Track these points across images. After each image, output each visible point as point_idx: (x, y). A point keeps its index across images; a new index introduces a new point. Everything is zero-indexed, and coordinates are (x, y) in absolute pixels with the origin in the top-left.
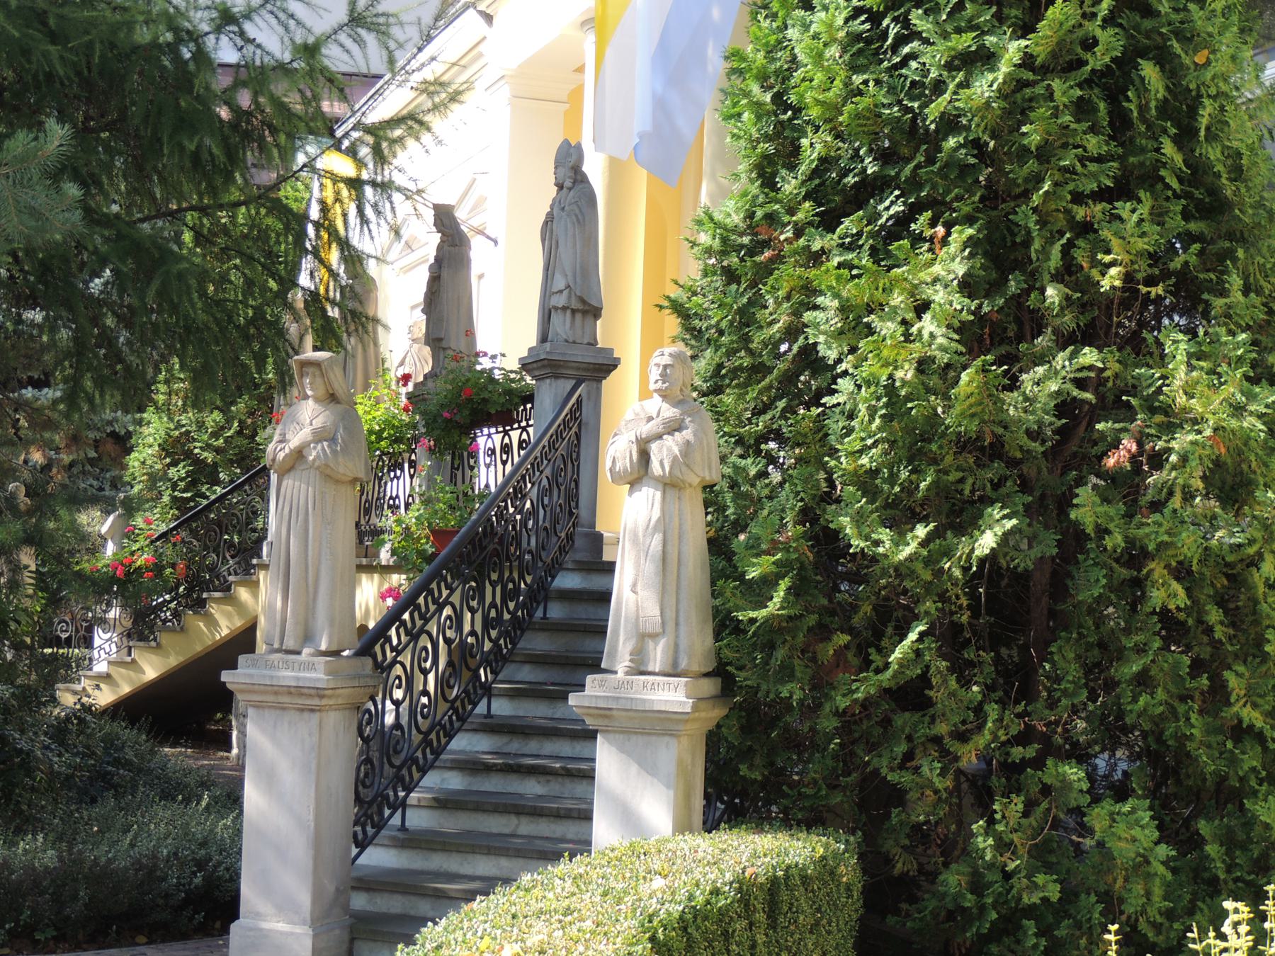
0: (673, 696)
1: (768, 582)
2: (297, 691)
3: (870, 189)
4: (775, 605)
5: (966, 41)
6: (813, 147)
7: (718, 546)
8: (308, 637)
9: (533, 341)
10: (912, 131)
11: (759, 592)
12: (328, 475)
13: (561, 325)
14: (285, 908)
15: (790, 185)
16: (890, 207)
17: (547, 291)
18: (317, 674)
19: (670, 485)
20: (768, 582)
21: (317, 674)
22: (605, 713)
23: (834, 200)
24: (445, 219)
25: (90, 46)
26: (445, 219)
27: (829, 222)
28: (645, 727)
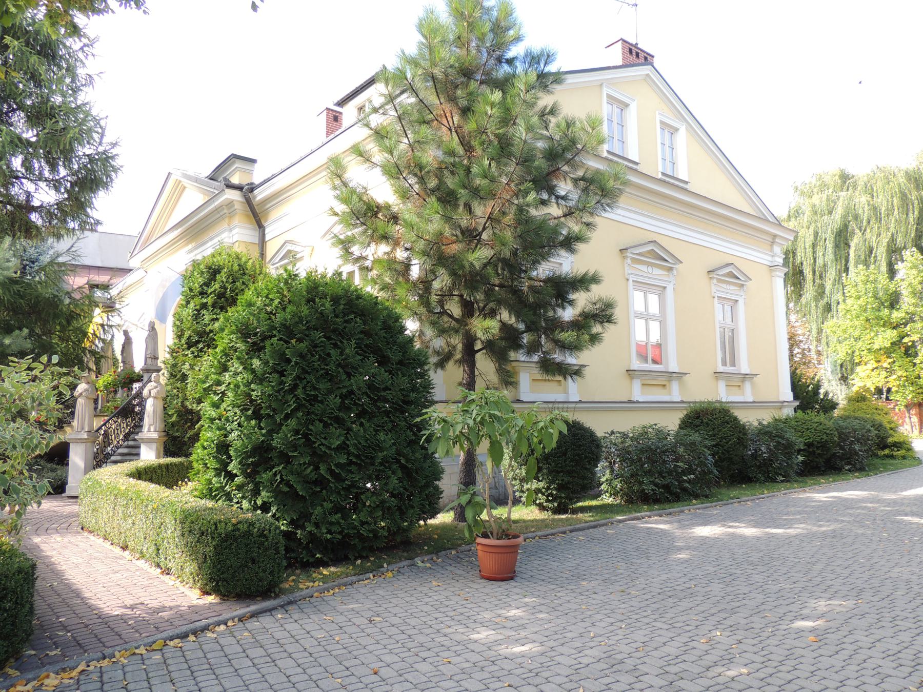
0: (155, 435)
1: (173, 415)
2: (81, 439)
3: (198, 342)
4: (174, 418)
5: (214, 316)
6: (187, 335)
7: (165, 408)
8: (83, 429)
9: (143, 364)
10: (205, 332)
11: (171, 416)
12: (87, 397)
13: (149, 361)
14: (75, 464)
15: (183, 341)
16: (200, 346)
17: (146, 354)
18: (85, 436)
19: (155, 398)
20: (173, 415)
21: (85, 436)
22: (142, 439)
23: (190, 345)
24: (126, 333)
25: (31, 300)
26: (126, 333)
27: (189, 348)
28: (149, 441)
